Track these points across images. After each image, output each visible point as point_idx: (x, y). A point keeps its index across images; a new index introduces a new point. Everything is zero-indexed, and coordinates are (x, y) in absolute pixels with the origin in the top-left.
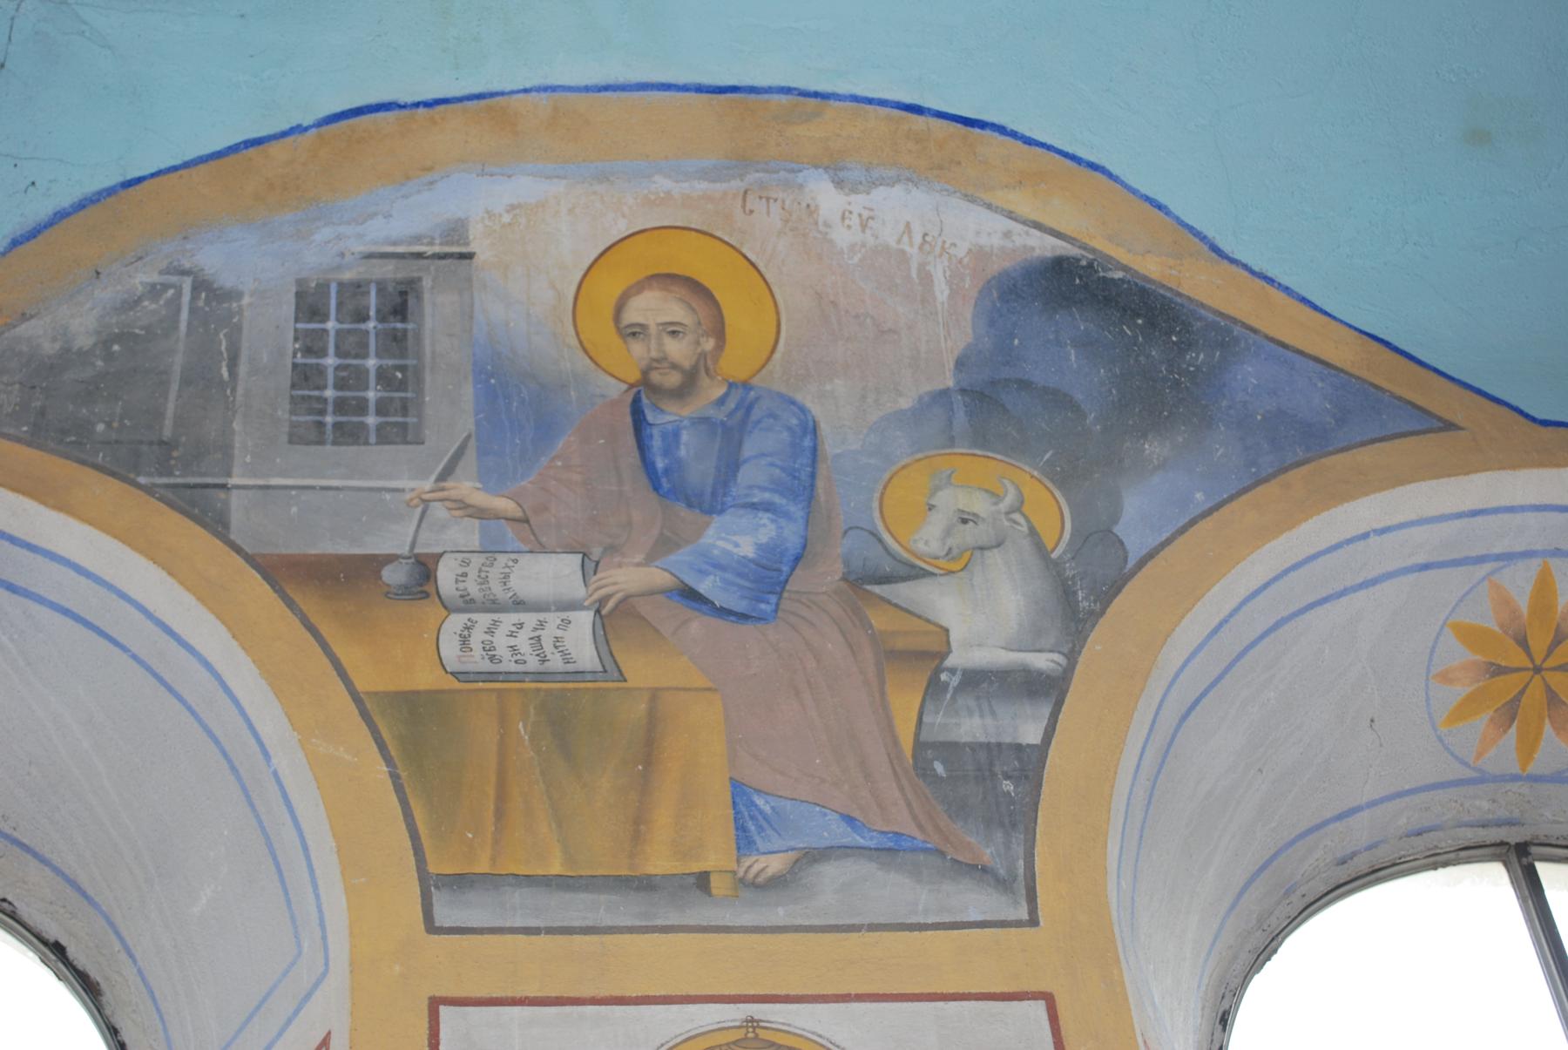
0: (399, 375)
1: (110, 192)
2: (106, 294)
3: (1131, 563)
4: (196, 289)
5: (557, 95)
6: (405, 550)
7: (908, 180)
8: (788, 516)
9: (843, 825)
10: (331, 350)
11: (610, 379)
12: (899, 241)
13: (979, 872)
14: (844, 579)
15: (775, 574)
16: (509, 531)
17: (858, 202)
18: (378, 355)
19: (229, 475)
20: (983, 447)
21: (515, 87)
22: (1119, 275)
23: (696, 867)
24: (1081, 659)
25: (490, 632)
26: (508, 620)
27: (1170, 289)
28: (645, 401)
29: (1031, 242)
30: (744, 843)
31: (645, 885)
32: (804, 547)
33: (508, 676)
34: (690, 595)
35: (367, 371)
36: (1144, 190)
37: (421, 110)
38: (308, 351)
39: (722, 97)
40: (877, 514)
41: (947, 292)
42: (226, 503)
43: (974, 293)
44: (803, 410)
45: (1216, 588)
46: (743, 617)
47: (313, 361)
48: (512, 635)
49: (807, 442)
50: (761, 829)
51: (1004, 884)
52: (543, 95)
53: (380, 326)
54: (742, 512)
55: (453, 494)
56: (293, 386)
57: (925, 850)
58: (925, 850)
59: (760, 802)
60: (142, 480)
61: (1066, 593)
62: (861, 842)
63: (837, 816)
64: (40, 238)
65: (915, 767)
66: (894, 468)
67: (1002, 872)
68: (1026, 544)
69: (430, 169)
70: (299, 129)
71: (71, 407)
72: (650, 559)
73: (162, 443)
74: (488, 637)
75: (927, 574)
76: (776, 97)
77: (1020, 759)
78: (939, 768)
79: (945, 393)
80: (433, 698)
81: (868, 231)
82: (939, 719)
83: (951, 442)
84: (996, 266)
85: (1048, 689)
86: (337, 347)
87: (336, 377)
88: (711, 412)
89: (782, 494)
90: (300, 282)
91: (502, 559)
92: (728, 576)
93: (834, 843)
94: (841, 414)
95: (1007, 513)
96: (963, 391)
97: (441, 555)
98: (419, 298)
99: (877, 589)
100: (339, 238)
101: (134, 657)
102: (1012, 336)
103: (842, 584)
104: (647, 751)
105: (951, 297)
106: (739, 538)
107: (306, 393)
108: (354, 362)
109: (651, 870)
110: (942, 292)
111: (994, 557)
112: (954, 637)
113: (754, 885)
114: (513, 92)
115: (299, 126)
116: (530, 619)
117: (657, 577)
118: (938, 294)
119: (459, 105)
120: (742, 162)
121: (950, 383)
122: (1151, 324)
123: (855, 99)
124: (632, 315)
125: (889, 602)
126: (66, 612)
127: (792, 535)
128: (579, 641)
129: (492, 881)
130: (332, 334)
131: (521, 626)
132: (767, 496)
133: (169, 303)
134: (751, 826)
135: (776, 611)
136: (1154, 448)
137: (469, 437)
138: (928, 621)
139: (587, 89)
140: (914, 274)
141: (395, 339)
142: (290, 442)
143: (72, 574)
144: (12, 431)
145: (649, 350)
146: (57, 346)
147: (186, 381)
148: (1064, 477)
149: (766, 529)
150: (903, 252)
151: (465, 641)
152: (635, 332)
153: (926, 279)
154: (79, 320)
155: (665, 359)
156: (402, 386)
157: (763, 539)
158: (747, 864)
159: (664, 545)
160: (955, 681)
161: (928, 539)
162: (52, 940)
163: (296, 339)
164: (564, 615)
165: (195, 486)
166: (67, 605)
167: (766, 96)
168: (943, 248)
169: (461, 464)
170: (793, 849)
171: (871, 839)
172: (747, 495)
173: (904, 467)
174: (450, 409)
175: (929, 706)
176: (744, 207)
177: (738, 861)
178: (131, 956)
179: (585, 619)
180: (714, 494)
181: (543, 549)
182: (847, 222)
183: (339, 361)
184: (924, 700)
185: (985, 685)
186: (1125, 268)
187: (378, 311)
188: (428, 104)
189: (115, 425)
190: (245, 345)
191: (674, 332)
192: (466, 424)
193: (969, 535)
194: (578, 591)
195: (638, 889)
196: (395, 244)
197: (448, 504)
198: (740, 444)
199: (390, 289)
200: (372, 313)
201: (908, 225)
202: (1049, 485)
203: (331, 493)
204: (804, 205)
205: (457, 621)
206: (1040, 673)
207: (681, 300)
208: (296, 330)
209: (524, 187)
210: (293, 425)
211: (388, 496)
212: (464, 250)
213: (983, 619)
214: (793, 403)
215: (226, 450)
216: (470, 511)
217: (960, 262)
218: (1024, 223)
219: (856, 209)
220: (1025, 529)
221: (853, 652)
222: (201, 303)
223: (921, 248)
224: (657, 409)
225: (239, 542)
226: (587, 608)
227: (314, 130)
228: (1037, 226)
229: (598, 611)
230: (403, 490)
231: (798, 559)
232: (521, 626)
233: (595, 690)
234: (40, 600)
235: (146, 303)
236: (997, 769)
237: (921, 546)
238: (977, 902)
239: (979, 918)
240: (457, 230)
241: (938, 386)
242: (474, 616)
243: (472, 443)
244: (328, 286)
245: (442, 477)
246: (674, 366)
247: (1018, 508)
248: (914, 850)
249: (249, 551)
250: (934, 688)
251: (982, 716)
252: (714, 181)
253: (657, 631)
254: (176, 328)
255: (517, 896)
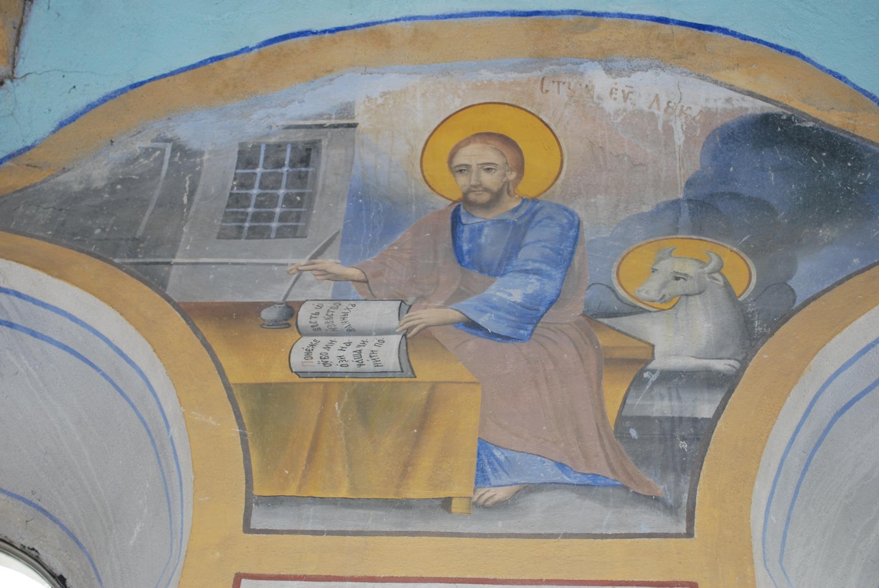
0: (299, 198)
1: (123, 91)
2: (117, 154)
3: (797, 304)
4: (174, 150)
5: (416, 22)
6: (281, 299)
7: (658, 66)
8: (549, 277)
9: (556, 469)
10: (257, 185)
11: (440, 198)
12: (650, 107)
13: (653, 501)
14: (584, 315)
15: (534, 312)
16: (353, 288)
17: (622, 83)
18: (287, 187)
19: (174, 257)
20: (699, 234)
21: (389, 19)
22: (811, 124)
23: (443, 494)
24: (751, 364)
25: (327, 347)
26: (341, 340)
27: (848, 133)
28: (462, 210)
29: (745, 105)
30: (481, 478)
31: (404, 505)
32: (558, 296)
33: (334, 375)
34: (472, 326)
35: (278, 196)
36: (829, 66)
37: (327, 35)
38: (242, 186)
39: (529, 18)
40: (614, 276)
41: (683, 139)
42: (168, 273)
43: (703, 139)
44: (572, 214)
45: (862, 319)
46: (507, 338)
47: (244, 191)
48: (342, 349)
49: (572, 233)
50: (495, 470)
51: (671, 510)
52: (408, 22)
53: (291, 170)
54: (517, 275)
55: (319, 266)
56: (228, 206)
57: (614, 486)
58: (614, 486)
59: (497, 453)
60: (117, 260)
61: (746, 323)
62: (568, 480)
63: (552, 463)
64: (77, 121)
65: (616, 432)
66: (631, 248)
67: (670, 501)
68: (721, 292)
69: (330, 71)
70: (247, 50)
71: (82, 220)
72: (446, 305)
73: (134, 239)
74: (325, 351)
75: (644, 311)
76: (566, 17)
77: (694, 427)
78: (633, 433)
79: (676, 202)
80: (280, 387)
81: (628, 101)
82: (639, 401)
83: (676, 231)
84: (719, 122)
85: (726, 383)
86: (261, 183)
87: (257, 200)
88: (507, 216)
89: (548, 264)
90: (241, 145)
91: (345, 304)
92: (501, 313)
93: (546, 481)
94: (597, 216)
95: (709, 273)
96: (689, 201)
97: (304, 302)
98: (318, 152)
99: (606, 321)
100: (268, 116)
101: (103, 375)
102: (729, 165)
103: (581, 318)
104: (423, 420)
105: (686, 142)
106: (513, 290)
107: (236, 210)
108: (269, 191)
109: (410, 495)
110: (679, 138)
111: (697, 301)
112: (657, 350)
113: (484, 507)
114: (388, 21)
115: (247, 47)
116: (356, 340)
117: (452, 314)
118: (676, 140)
119: (351, 31)
120: (540, 58)
121: (681, 196)
122: (833, 155)
123: (621, 15)
124: (461, 159)
125: (614, 329)
126: (65, 348)
127: (550, 289)
128: (389, 353)
129: (296, 501)
130: (259, 176)
131: (349, 344)
132: (537, 265)
133: (155, 160)
134: (488, 469)
135: (531, 335)
136: (825, 233)
137: (338, 233)
138: (640, 340)
139: (437, 17)
140: (660, 128)
141: (300, 177)
142: (218, 238)
143: (68, 321)
144: (41, 234)
145: (470, 180)
146: (82, 187)
147: (159, 205)
148: (753, 252)
149: (533, 285)
150: (653, 114)
151: (308, 353)
152: (463, 170)
153: (668, 130)
154: (98, 171)
155: (481, 185)
156: (300, 204)
157: (530, 290)
158: (481, 493)
159: (459, 295)
160: (654, 377)
161: (649, 290)
162: (58, 574)
163: (235, 179)
164: (380, 338)
165: (150, 263)
166: (66, 343)
167: (559, 17)
168: (681, 110)
169: (329, 249)
170: (516, 484)
171: (575, 478)
172: (522, 265)
173: (639, 247)
174: (329, 216)
175: (632, 393)
176: (542, 88)
177: (475, 491)
178: (100, 580)
179: (394, 340)
180: (500, 265)
181: (375, 298)
182: (614, 96)
183: (261, 191)
184: (629, 390)
185: (676, 380)
186: (815, 120)
187: (291, 161)
188: (331, 31)
189: (107, 230)
190: (201, 183)
191: (488, 169)
192: (338, 225)
193: (679, 287)
194: (394, 323)
195: (399, 508)
196: (305, 119)
197: (315, 272)
198: (524, 235)
199: (300, 147)
200: (287, 162)
201: (657, 95)
202: (743, 255)
203: (238, 266)
204: (584, 86)
205: (306, 341)
206: (718, 372)
207: (495, 149)
208: (236, 174)
209: (392, 81)
210: (223, 228)
211: (276, 268)
212: (350, 122)
213: (681, 338)
214: (566, 210)
215: (175, 244)
216: (329, 276)
217: (694, 119)
218: (741, 92)
219: (620, 87)
220: (722, 283)
221: (582, 360)
222: (176, 159)
223: (665, 111)
224: (469, 214)
225: (171, 295)
226: (398, 333)
227: (256, 50)
228: (751, 94)
229: (405, 335)
230: (287, 265)
231: (552, 303)
232: (349, 344)
233: (393, 382)
234: (50, 341)
235: (142, 160)
236: (677, 434)
237: (643, 294)
238: (648, 520)
239: (648, 531)
240: (347, 109)
241: (672, 197)
242: (318, 338)
243: (340, 237)
244: (260, 147)
245: (315, 257)
246: (486, 190)
247: (718, 270)
248: (605, 486)
249: (176, 300)
250: (638, 382)
251: (670, 400)
252: (521, 72)
253: (443, 347)
254: (159, 174)
255: (311, 510)
